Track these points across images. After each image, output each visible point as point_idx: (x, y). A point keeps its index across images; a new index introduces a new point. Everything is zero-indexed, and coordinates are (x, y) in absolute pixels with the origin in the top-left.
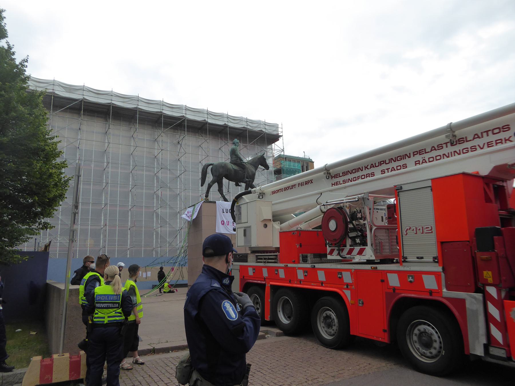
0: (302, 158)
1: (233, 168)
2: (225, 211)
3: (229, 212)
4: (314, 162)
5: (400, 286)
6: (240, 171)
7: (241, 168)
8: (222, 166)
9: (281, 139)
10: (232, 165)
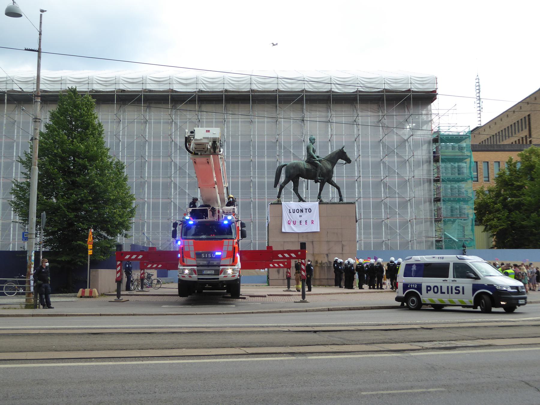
2: (291, 211)
3: (296, 212)
5: (401, 303)
8: (293, 166)
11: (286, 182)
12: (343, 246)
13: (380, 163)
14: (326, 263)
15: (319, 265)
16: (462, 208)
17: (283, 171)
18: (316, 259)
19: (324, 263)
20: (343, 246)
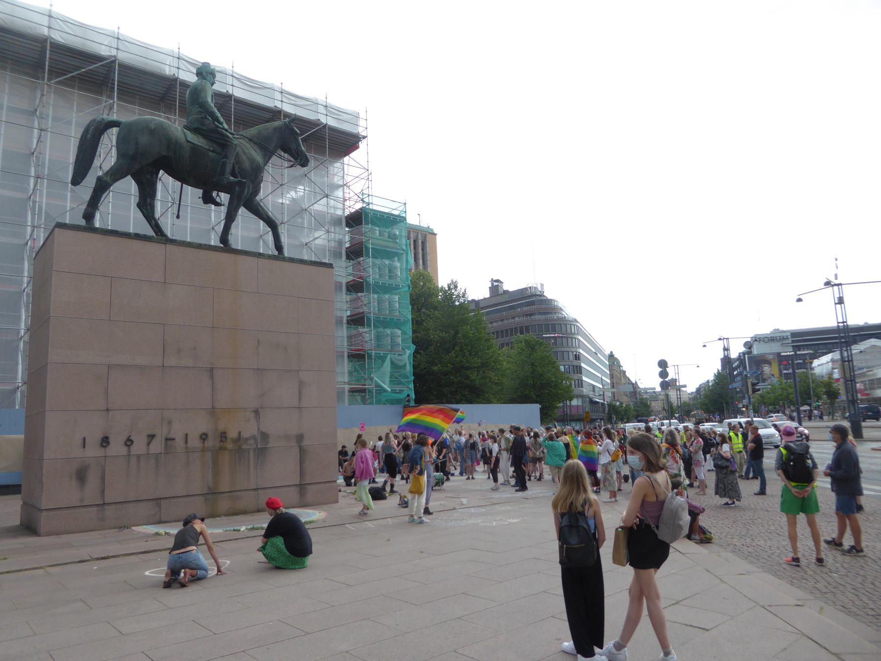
0: (416, 225)
1: (186, 139)
4: (436, 234)
6: (213, 151)
7: (215, 142)
9: (362, 145)
10: (185, 130)
11: (116, 174)
12: (301, 384)
13: (259, 242)
14: (254, 437)
15: (230, 445)
16: (395, 335)
17: (110, 139)
18: (222, 426)
19: (247, 439)
20: (301, 384)
